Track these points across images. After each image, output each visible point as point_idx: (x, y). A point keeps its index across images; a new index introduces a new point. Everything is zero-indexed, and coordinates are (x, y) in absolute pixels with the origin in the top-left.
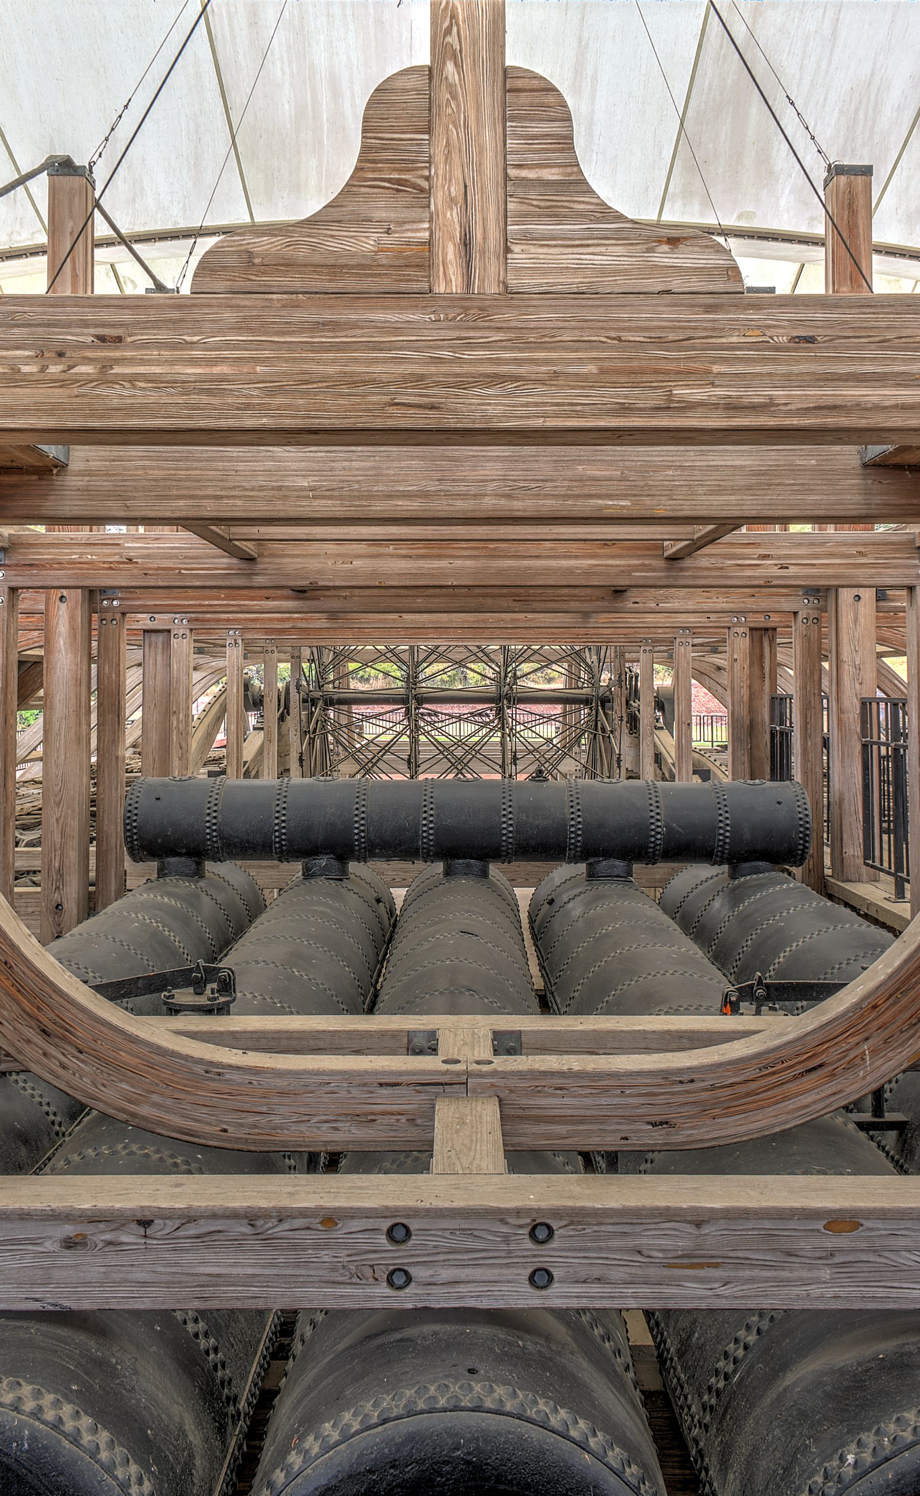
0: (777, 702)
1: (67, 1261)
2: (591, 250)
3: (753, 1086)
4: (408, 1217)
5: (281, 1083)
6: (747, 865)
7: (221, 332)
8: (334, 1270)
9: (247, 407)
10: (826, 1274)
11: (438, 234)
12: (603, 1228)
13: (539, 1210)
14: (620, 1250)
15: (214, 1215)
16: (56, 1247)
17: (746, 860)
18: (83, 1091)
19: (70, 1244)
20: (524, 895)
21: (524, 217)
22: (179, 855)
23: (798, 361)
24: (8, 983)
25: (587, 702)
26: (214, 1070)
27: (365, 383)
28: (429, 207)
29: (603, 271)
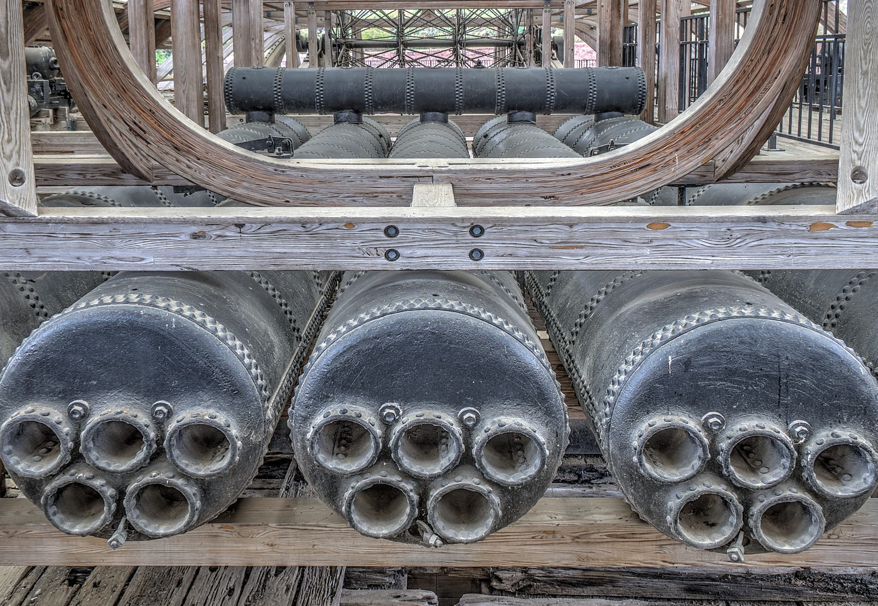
0: (628, 30)
1: (194, 245)
3: (606, 177)
4: (397, 222)
6: (606, 114)
8: (354, 250)
10: (648, 251)
12: (514, 228)
13: (475, 219)
14: (524, 239)
16: (188, 238)
17: (605, 111)
18: (201, 180)
19: (195, 236)
22: (258, 110)
24: (153, 122)
25: (509, 45)
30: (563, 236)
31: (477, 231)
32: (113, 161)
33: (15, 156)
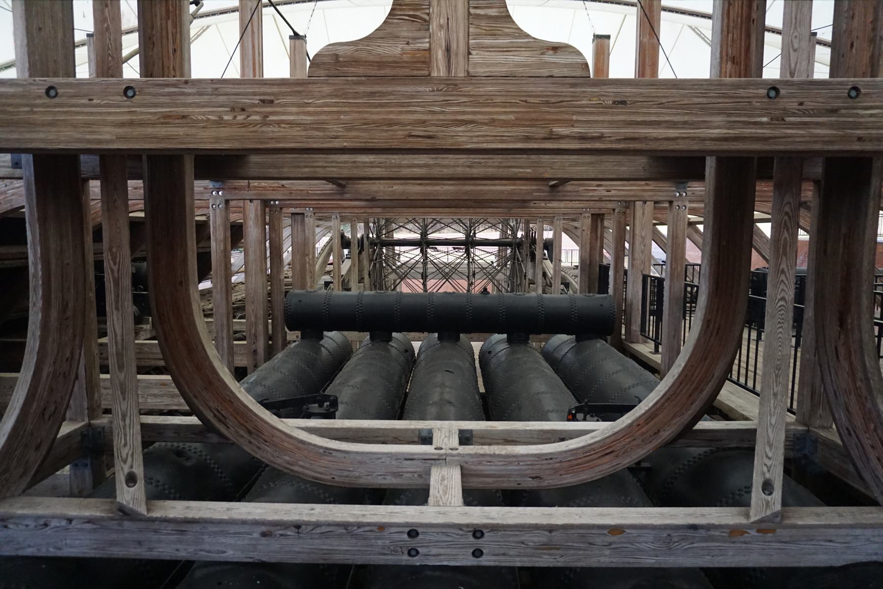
1: (264, 542)
2: (512, 53)
3: (580, 461)
5: (359, 458)
7: (324, 97)
9: (336, 137)
10: (607, 552)
11: (433, 46)
15: (329, 524)
19: (264, 535)
20: (477, 346)
21: (478, 36)
23: (618, 114)
25: (509, 244)
26: (328, 451)
27: (396, 124)
28: (429, 30)
29: (518, 65)
30: (544, 539)
31: (478, 535)
32: (200, 423)
33: (130, 459)
